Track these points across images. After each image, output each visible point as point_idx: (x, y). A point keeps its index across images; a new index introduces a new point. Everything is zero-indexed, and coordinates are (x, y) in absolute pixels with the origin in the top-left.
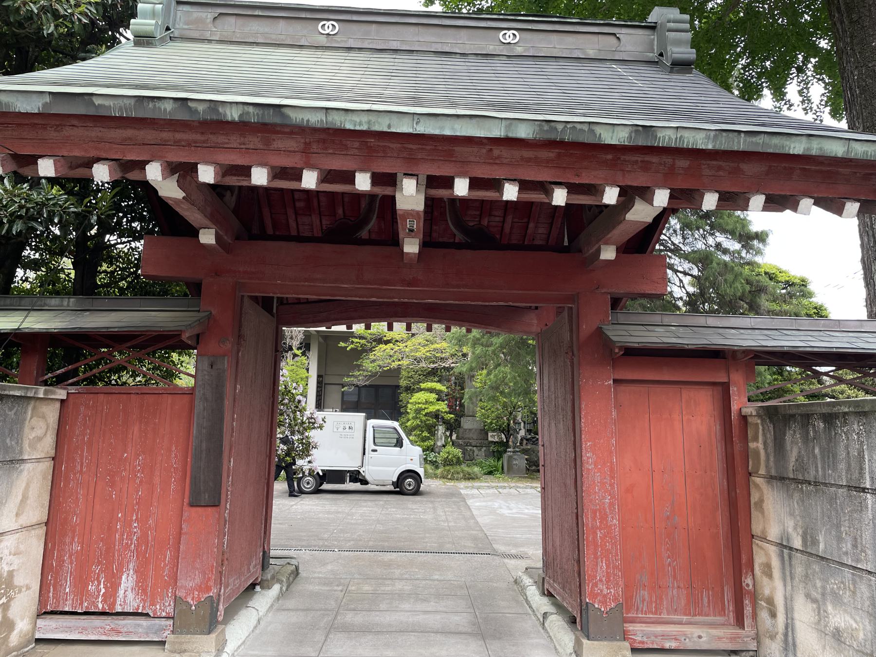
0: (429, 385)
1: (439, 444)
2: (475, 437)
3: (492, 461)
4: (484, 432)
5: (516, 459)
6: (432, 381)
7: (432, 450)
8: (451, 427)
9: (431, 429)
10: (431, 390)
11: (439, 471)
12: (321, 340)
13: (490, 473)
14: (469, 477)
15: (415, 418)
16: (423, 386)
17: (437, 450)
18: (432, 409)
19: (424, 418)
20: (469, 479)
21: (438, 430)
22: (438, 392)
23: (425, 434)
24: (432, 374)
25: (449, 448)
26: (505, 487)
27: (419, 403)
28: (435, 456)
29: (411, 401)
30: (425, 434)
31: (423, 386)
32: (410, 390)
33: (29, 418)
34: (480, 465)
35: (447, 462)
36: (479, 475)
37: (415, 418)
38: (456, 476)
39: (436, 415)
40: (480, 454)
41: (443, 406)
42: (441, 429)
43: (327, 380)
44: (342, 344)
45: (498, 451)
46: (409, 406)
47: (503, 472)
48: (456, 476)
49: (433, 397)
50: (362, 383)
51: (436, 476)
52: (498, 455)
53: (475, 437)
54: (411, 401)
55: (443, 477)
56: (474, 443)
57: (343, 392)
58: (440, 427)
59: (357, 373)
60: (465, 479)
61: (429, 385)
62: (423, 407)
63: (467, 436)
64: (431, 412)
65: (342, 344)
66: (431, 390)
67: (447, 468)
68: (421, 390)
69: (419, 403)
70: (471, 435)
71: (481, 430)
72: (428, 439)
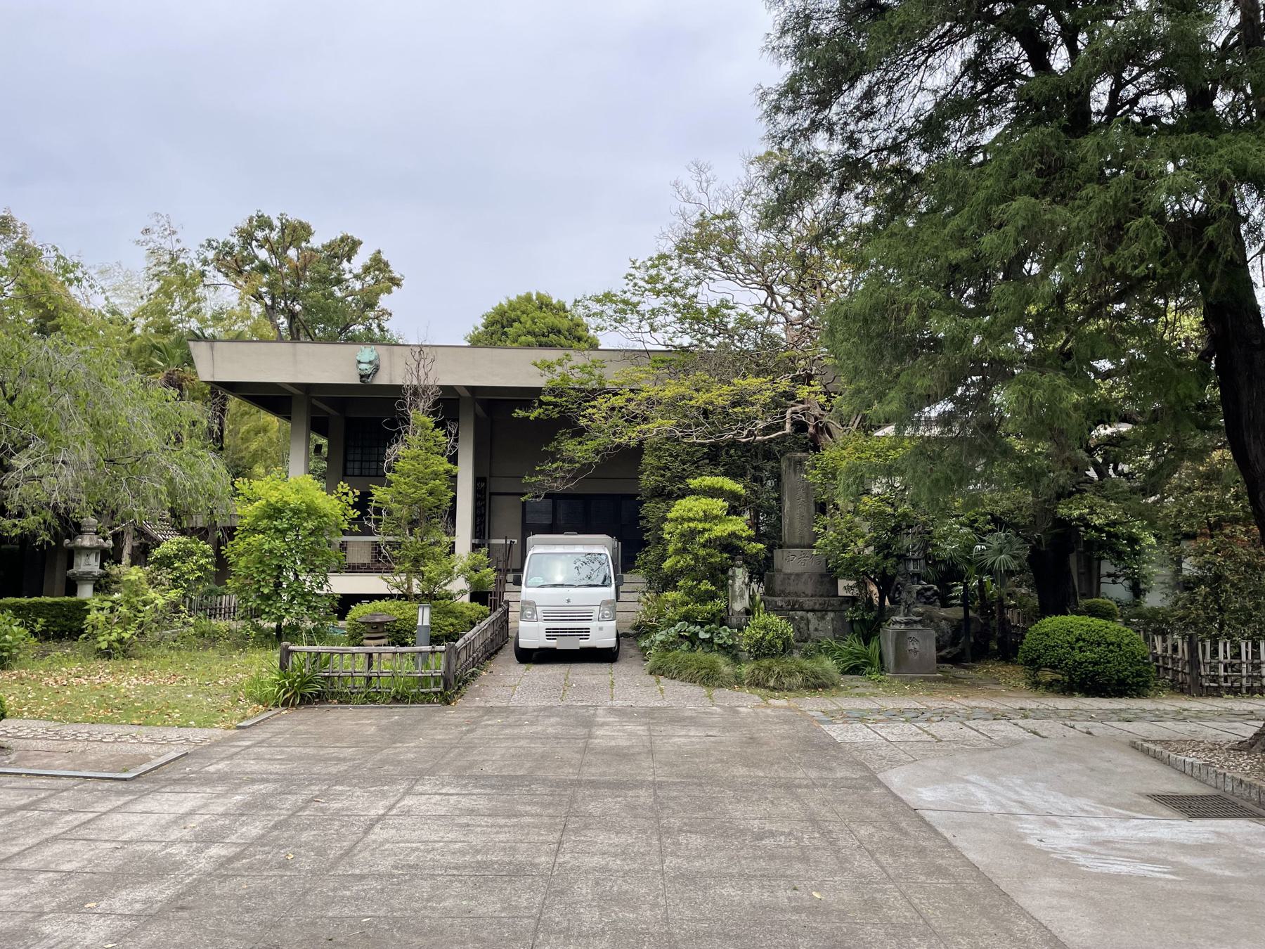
0: (709, 481)
1: (738, 606)
2: (809, 592)
3: (854, 644)
4: (829, 578)
5: (914, 640)
6: (712, 474)
7: (723, 622)
8: (761, 570)
9: (719, 575)
10: (713, 493)
11: (746, 669)
12: (479, 409)
13: (854, 670)
14: (817, 684)
15: (682, 551)
16: (694, 483)
17: (734, 620)
18: (719, 530)
19: (702, 552)
20: (816, 687)
21: (733, 577)
22: (731, 496)
23: (706, 586)
24: (714, 457)
25: (761, 618)
26: (943, 715)
27: (691, 520)
28: (731, 636)
29: (669, 516)
30: (706, 586)
31: (694, 483)
32: (667, 495)
33: (1140, 729)
34: (829, 652)
35: (762, 650)
36: (836, 676)
37: (682, 551)
38: (786, 681)
39: (729, 546)
40: (822, 627)
41: (739, 525)
42: (740, 575)
43: (495, 485)
44: (519, 413)
45: (863, 621)
46: (667, 527)
47: (882, 669)
48: (786, 681)
49: (718, 506)
50: (559, 487)
51: (738, 681)
52: (869, 630)
53: (809, 592)
54: (669, 516)
55: (757, 684)
56: (808, 603)
57: (524, 504)
58: (739, 571)
59: (550, 466)
60: (807, 687)
61: (709, 481)
62: (700, 526)
63: (791, 589)
64: (717, 538)
65: (519, 413)
66: (713, 493)
67: (766, 662)
68: (693, 492)
69: (691, 520)
70: (800, 587)
71: (822, 575)
72: (712, 596)
